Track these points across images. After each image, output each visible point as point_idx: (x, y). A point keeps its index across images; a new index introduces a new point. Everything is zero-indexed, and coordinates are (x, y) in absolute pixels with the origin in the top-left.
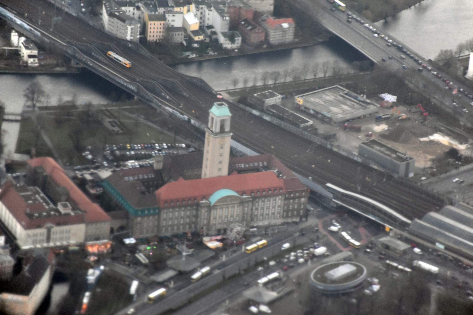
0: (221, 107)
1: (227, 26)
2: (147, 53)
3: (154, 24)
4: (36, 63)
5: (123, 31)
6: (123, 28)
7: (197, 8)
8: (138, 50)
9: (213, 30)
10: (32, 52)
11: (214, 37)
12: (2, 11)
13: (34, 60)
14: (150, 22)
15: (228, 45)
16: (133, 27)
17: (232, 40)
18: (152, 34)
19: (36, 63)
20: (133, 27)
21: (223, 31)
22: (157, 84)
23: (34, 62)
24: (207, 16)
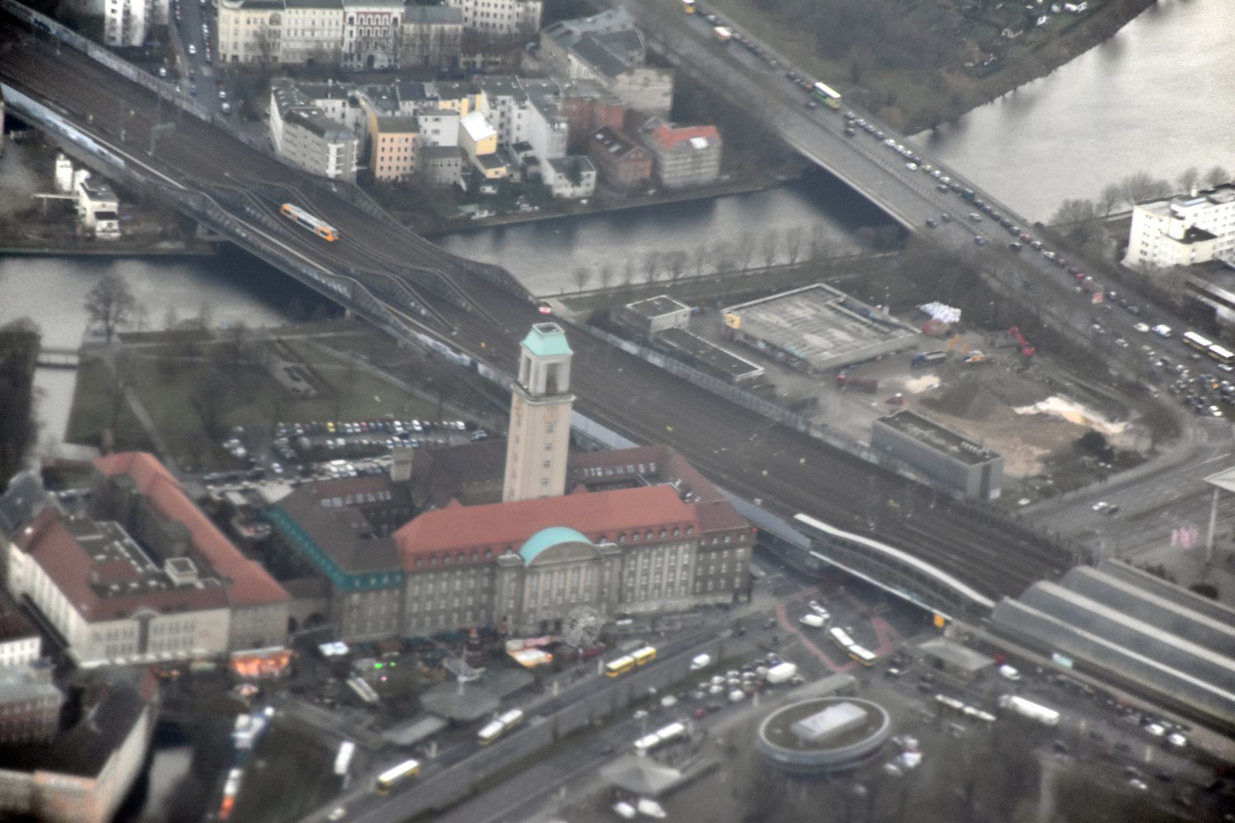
0: (548, 334)
1: (563, 145)
6: (318, 149)
7: (492, 101)
8: (353, 200)
9: (530, 153)
10: (104, 206)
13: (110, 225)
15: (563, 188)
16: (341, 145)
23: (109, 229)
24: (515, 122)
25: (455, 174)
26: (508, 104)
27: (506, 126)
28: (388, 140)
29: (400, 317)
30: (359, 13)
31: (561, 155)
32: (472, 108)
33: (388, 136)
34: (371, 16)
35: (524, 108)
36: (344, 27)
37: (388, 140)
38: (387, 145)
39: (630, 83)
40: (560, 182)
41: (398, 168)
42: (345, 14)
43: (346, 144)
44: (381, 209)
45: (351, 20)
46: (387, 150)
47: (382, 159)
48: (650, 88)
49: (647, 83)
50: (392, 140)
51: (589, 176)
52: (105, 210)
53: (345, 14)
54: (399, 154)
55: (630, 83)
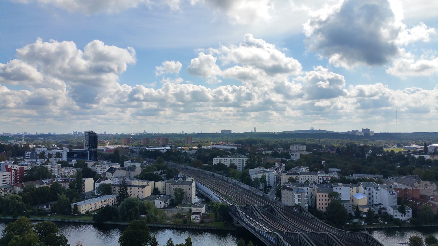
0: (370, 67)
1: (396, 200)
2: (308, 214)
3: (322, 196)
4: (198, 220)
5: (291, 200)
6: (291, 197)
7: (365, 188)
8: (301, 213)
9: (382, 206)
10: (197, 210)
11: (383, 211)
12: (21, 68)
13: (196, 217)
14: (318, 194)
15: (398, 216)
16: (300, 194)
17: (402, 211)
18: (321, 202)
19: (198, 220)
20: (300, 194)
21: (392, 205)
22: (303, 235)
23: (196, 219)
24: (375, 195)
25: (350, 210)
26: (371, 190)
27: (372, 199)
28: (321, 196)
29: (248, 218)
30: (323, 177)
31: (395, 204)
32: (357, 192)
33: (321, 194)
34: (327, 178)
35: (378, 190)
36: (318, 181)
37: (321, 196)
38: (321, 198)
39: (420, 186)
40: (396, 214)
41: (326, 204)
42: (318, 177)
43: (301, 194)
44: (311, 215)
45: (321, 179)
46: (321, 200)
47: (319, 204)
48: (428, 188)
49: (426, 186)
50: (322, 196)
51: (409, 212)
52: (197, 211)
53: (318, 177)
54: (323, 202)
55: (420, 186)
